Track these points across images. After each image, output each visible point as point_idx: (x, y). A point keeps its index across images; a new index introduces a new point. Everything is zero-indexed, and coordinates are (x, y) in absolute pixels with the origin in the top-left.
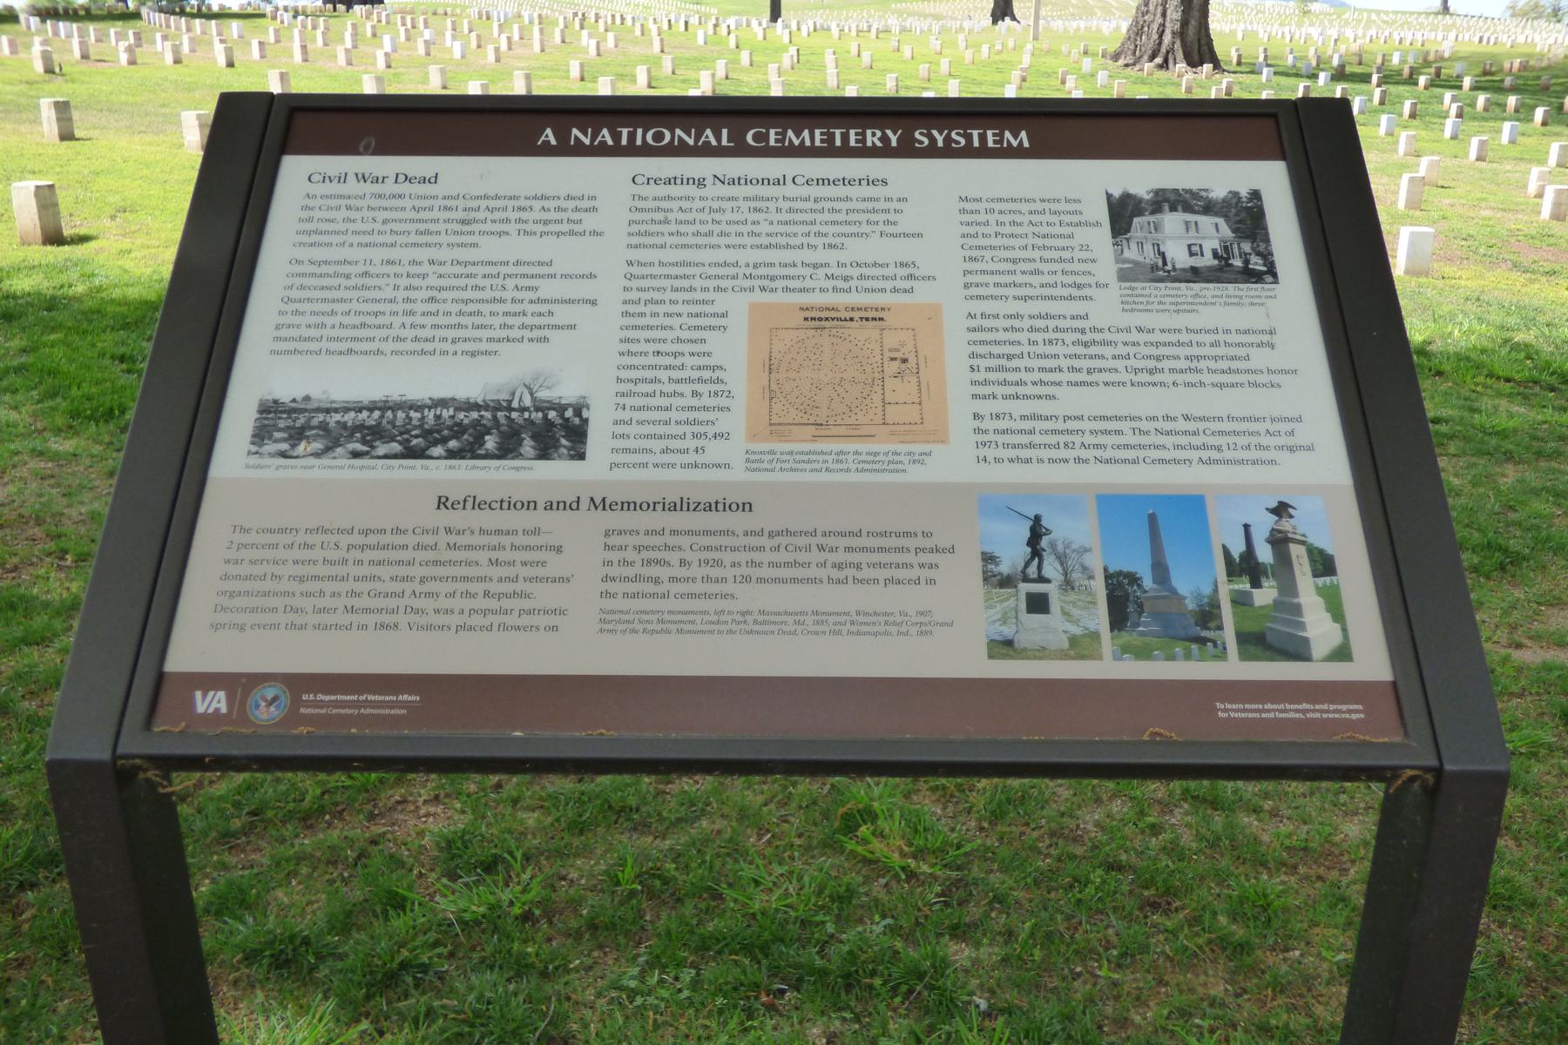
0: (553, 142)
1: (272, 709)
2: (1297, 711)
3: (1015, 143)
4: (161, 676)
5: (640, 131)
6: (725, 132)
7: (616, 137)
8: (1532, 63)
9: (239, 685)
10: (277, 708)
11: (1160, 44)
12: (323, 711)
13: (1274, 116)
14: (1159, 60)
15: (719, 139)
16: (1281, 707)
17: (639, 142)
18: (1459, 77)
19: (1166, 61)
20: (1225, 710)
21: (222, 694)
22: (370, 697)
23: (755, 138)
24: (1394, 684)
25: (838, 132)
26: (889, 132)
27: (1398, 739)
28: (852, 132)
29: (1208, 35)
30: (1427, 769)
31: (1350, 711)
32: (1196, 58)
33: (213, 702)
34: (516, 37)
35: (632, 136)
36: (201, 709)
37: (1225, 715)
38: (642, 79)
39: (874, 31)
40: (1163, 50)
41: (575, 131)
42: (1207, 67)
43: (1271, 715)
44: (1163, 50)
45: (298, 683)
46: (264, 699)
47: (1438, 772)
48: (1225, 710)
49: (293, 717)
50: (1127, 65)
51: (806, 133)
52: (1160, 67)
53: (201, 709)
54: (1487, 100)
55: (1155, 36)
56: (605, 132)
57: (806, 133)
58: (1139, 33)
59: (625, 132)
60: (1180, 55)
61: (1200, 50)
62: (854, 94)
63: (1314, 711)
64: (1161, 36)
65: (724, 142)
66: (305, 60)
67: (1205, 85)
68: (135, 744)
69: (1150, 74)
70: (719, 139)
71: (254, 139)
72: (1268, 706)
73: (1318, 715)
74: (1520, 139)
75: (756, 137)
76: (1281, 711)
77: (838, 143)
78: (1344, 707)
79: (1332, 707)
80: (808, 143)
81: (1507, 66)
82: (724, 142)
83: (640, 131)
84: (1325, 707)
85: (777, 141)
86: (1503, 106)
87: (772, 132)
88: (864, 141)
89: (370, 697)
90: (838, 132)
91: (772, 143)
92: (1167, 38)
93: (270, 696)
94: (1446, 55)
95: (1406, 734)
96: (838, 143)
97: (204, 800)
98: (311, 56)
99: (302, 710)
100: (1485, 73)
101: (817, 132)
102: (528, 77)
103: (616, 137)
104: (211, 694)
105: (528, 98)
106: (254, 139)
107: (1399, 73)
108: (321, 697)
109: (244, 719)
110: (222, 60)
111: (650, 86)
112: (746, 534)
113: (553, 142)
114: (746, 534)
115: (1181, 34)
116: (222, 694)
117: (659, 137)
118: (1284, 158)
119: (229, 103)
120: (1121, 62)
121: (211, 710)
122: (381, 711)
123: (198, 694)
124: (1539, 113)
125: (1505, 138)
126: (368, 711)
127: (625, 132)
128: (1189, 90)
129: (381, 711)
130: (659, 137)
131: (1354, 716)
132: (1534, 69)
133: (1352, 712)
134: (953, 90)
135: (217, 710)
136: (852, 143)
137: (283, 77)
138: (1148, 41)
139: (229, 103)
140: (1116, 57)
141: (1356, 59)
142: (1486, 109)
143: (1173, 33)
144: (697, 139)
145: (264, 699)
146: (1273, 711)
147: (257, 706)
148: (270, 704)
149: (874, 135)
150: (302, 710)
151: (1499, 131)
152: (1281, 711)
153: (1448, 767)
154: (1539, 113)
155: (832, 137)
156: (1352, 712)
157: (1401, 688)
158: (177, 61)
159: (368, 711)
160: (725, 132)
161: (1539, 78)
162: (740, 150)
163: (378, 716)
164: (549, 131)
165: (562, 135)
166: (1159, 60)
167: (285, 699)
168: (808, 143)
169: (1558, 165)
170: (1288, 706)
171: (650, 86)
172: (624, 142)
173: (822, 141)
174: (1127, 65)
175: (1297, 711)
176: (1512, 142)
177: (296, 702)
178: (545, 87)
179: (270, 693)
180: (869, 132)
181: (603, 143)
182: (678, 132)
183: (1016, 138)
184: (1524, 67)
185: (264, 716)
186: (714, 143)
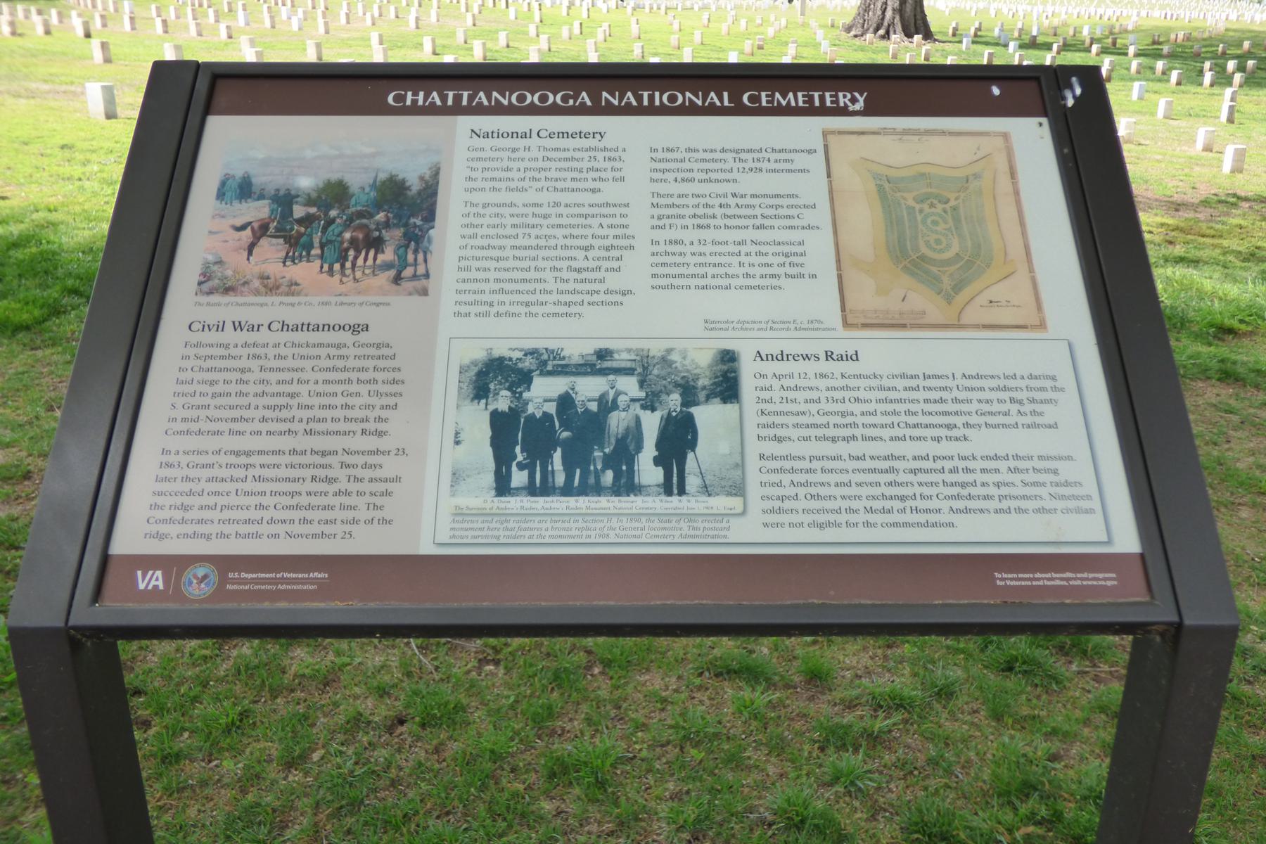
0: (589, 103)
1: (203, 586)
2: (1062, 579)
3: (784, 103)
4: (105, 559)
5: (657, 94)
6: (726, 95)
7: (639, 99)
8: (1195, 34)
9: (174, 565)
10: (207, 585)
11: (883, 19)
12: (247, 587)
13: (1037, 79)
14: (881, 32)
15: (721, 100)
16: (1049, 575)
17: (657, 103)
18: (1126, 47)
19: (888, 32)
20: (1002, 579)
21: (159, 573)
22: (287, 575)
23: (750, 99)
24: (1142, 556)
25: (816, 95)
26: (857, 95)
27: (1147, 599)
28: (827, 94)
29: (923, 11)
30: (1170, 624)
31: (1105, 579)
32: (913, 30)
33: (155, 580)
34: (376, 15)
35: (651, 98)
36: (142, 586)
37: (1002, 583)
38: (428, 47)
39: (663, 8)
40: (886, 24)
41: (605, 94)
42: (917, 38)
43: (1041, 583)
44: (886, 24)
45: (225, 564)
46: (195, 576)
47: (1179, 626)
48: (1002, 579)
49: (220, 593)
50: (856, 36)
51: (791, 95)
52: (883, 37)
53: (142, 586)
54: (1139, 64)
55: (879, 13)
56: (435, 94)
57: (791, 95)
58: (867, 10)
59: (646, 94)
60: (899, 27)
61: (916, 24)
62: (735, 61)
63: (1075, 579)
64: (884, 11)
65: (726, 103)
66: (166, 32)
67: (907, 51)
68: (85, 615)
69: (871, 43)
70: (721, 100)
71: (184, 99)
72: (1038, 575)
73: (1078, 583)
74: (1147, 95)
75: (751, 99)
76: (1049, 579)
77: (817, 104)
78: (1101, 576)
79: (1091, 575)
80: (793, 104)
81: (1173, 37)
82: (726, 103)
83: (657, 94)
84: (1085, 575)
85: (768, 102)
86: (1152, 69)
87: (763, 94)
88: (837, 102)
89: (287, 575)
90: (816, 95)
91: (764, 104)
92: (889, 14)
93: (200, 574)
94: (1130, 28)
95: (1152, 597)
96: (817, 104)
97: (146, 663)
98: (170, 30)
99: (229, 587)
100: (1154, 43)
101: (800, 94)
102: (318, 46)
103: (639, 99)
104: (150, 573)
105: (989, 67)
106: (184, 99)
107: (1083, 42)
108: (244, 575)
109: (178, 595)
110: (80, 32)
111: (435, 53)
112: (915, 458)
113: (589, 103)
114: (915, 458)
115: (900, 11)
116: (159, 573)
117: (672, 99)
118: (1046, 115)
119: (161, 71)
120: (853, 33)
121: (150, 587)
122: (296, 587)
123: (139, 573)
124: (1174, 75)
125: (1135, 96)
126: (284, 587)
127: (646, 94)
128: (895, 56)
129: (296, 587)
130: (672, 99)
131: (1109, 583)
132: (1197, 40)
133: (1107, 579)
134: (787, 57)
135: (156, 587)
136: (828, 104)
137: (178, 48)
138: (873, 17)
139: (161, 71)
140: (848, 29)
141: (1051, 32)
142: (1138, 72)
143: (894, 10)
144: (704, 101)
145: (195, 576)
146: (1055, 579)
147: (191, 583)
148: (201, 581)
149: (845, 96)
150: (229, 587)
151: (1131, 90)
152: (1049, 579)
153: (1188, 622)
154: (1174, 75)
155: (811, 98)
156: (1107, 579)
157: (1148, 558)
158: (48, 32)
159: (284, 587)
160: (726, 95)
161: (1192, 47)
162: (738, 110)
163: (293, 590)
164: (584, 94)
165: (595, 98)
166: (881, 32)
167: (214, 578)
168: (793, 104)
169: (1165, 117)
170: (1055, 575)
171: (435, 53)
172: (646, 103)
173: (804, 102)
174: (856, 36)
175: (1062, 579)
176: (1141, 98)
177: (224, 580)
178: (339, 54)
179: (201, 572)
180: (841, 95)
181: (629, 104)
182: (688, 94)
183: (784, 97)
184: (1188, 38)
185: (197, 592)
186: (718, 104)
